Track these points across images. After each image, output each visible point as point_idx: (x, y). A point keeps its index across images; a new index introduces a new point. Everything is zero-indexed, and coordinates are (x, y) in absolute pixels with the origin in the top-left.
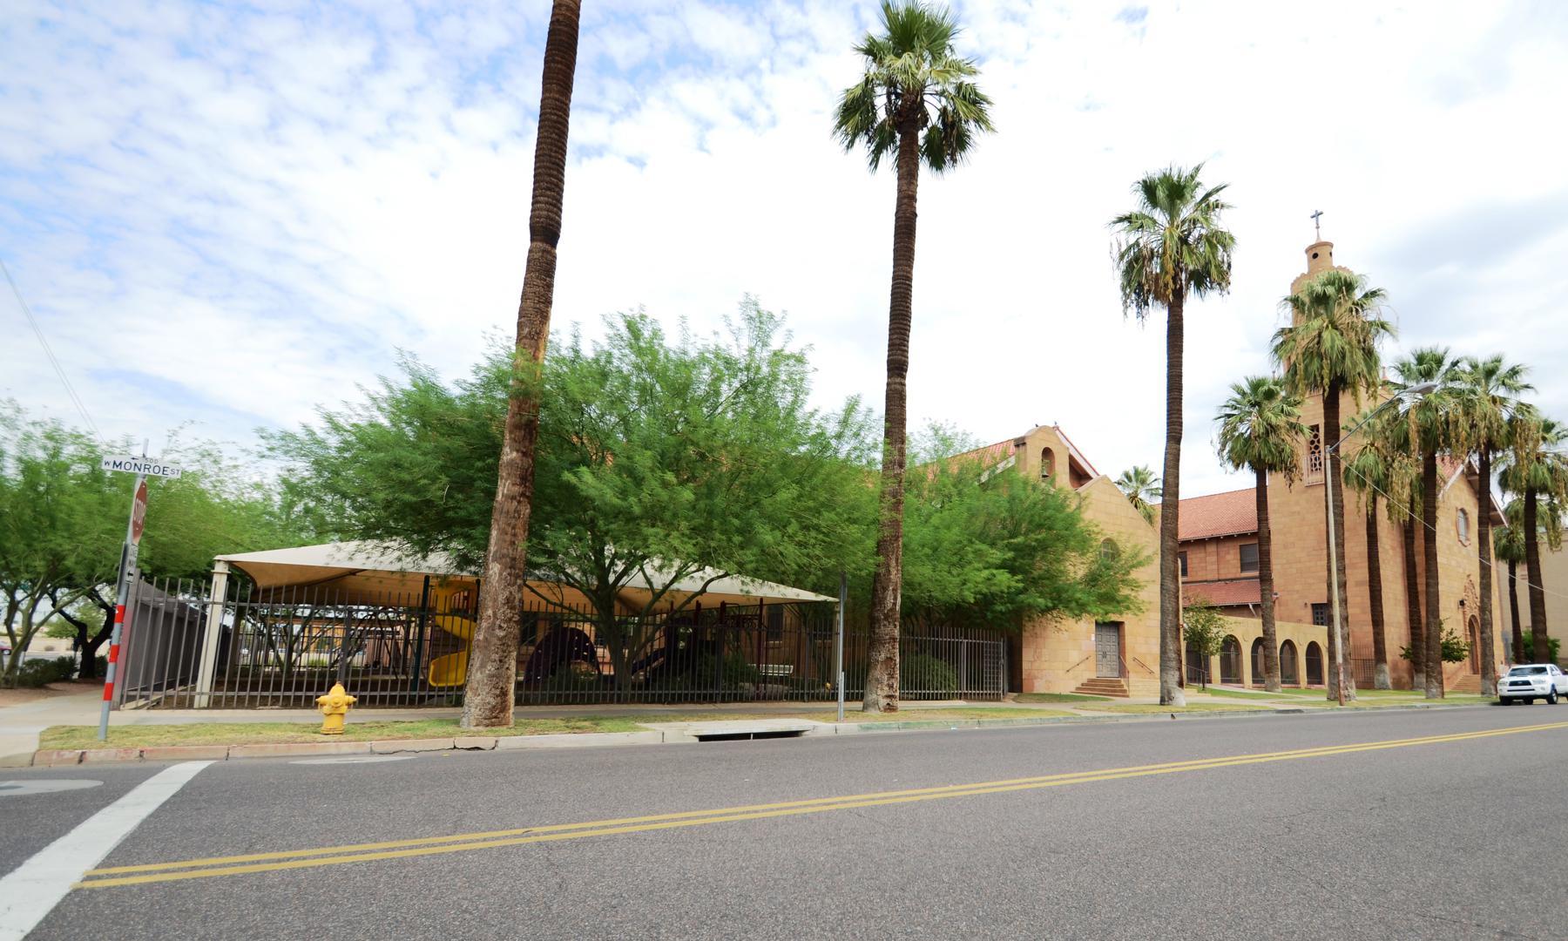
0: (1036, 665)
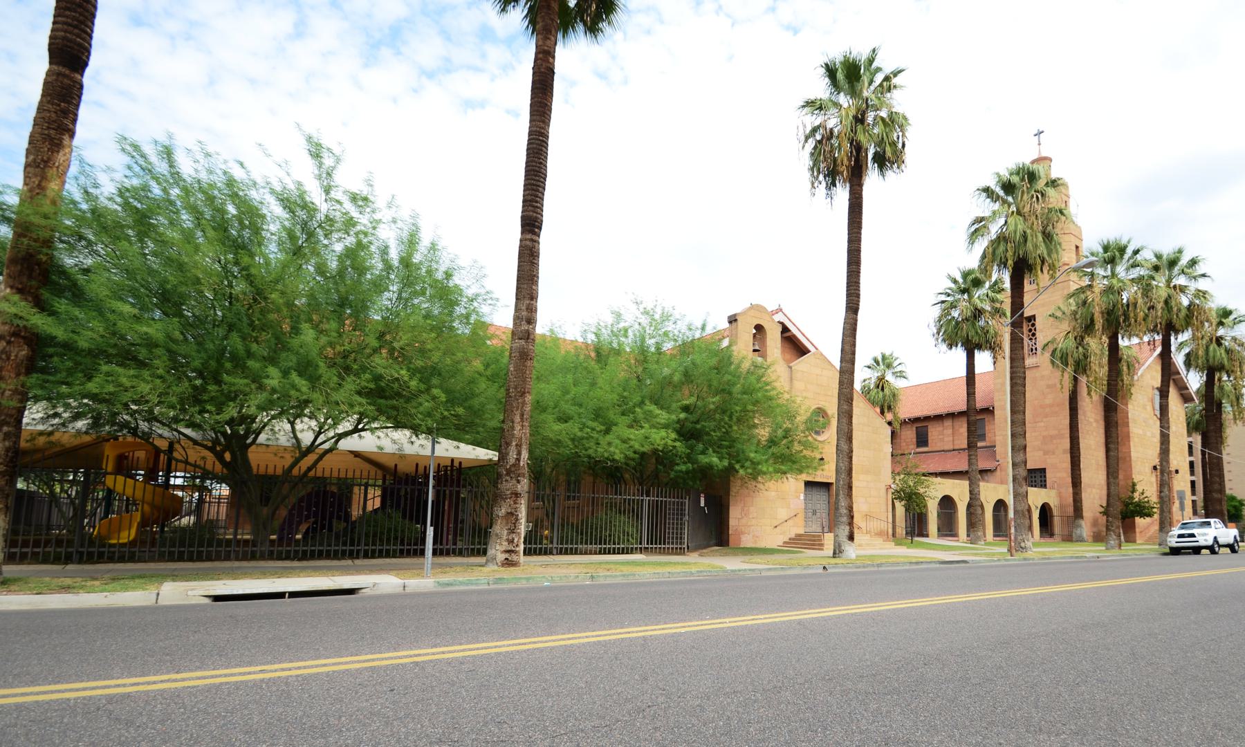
0: (744, 521)
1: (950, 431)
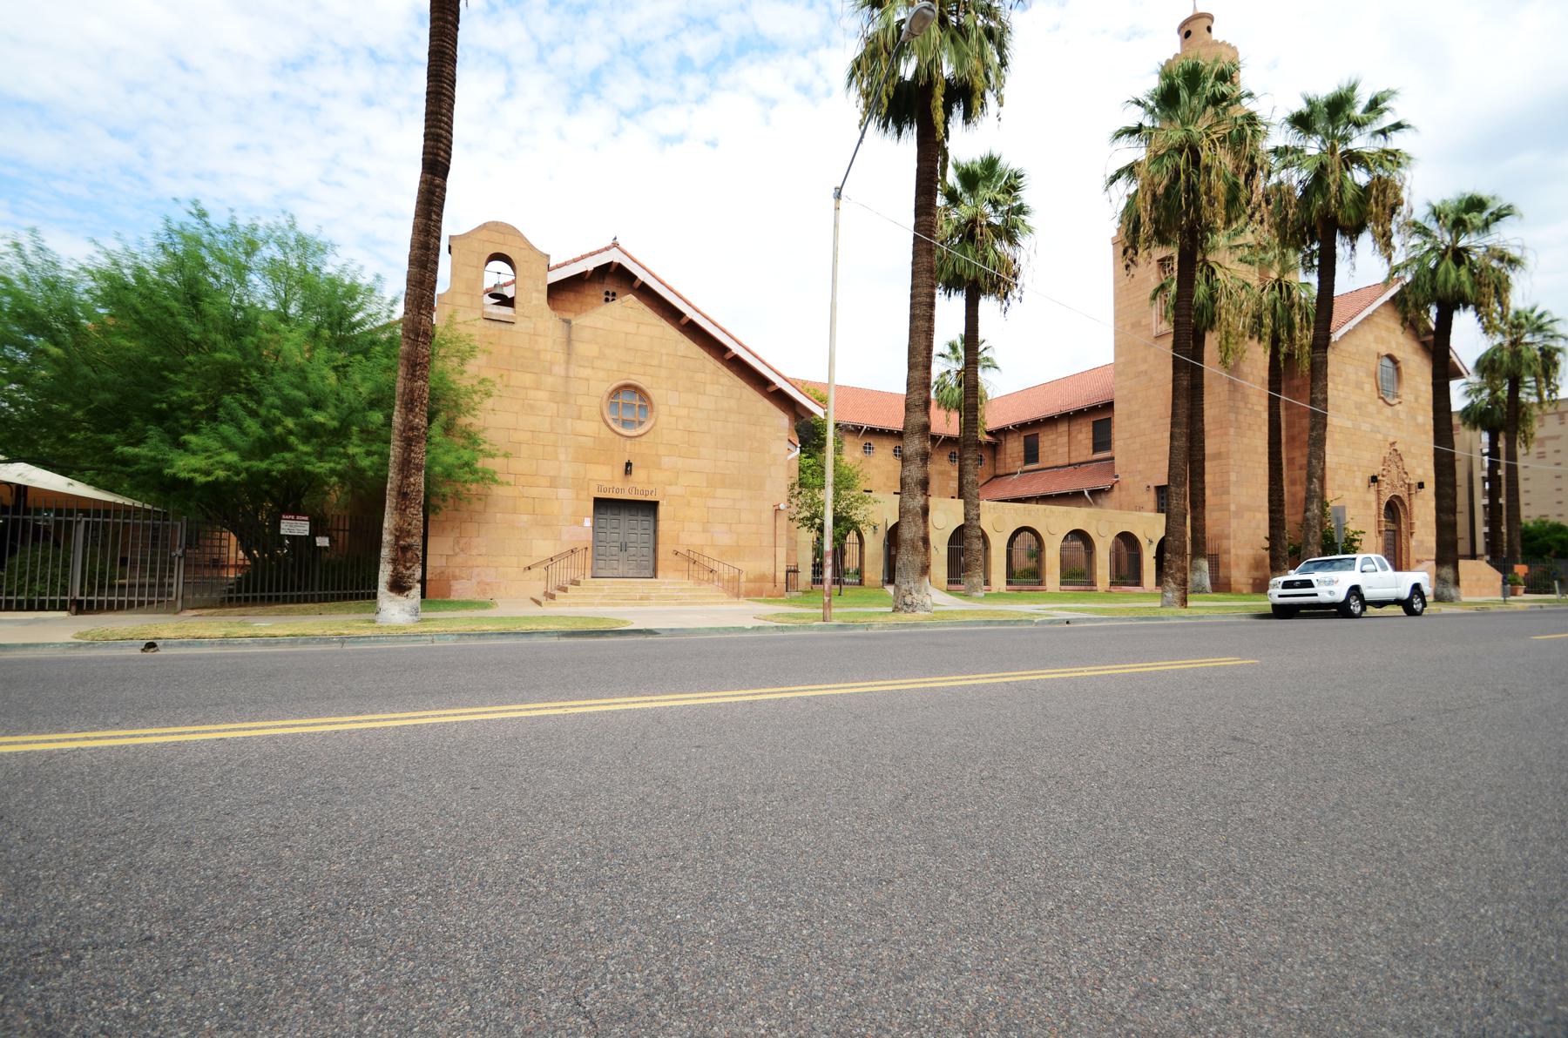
0: (459, 559)
1: (1065, 439)
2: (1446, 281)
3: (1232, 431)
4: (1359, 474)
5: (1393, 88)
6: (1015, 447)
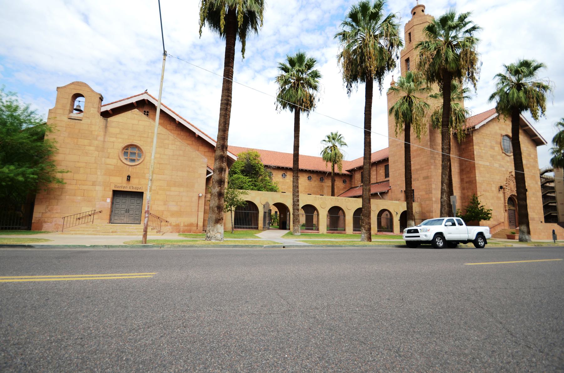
0: (48, 214)
2: (513, 97)
3: (432, 167)
4: (494, 185)
5: (469, 11)
6: (358, 176)
